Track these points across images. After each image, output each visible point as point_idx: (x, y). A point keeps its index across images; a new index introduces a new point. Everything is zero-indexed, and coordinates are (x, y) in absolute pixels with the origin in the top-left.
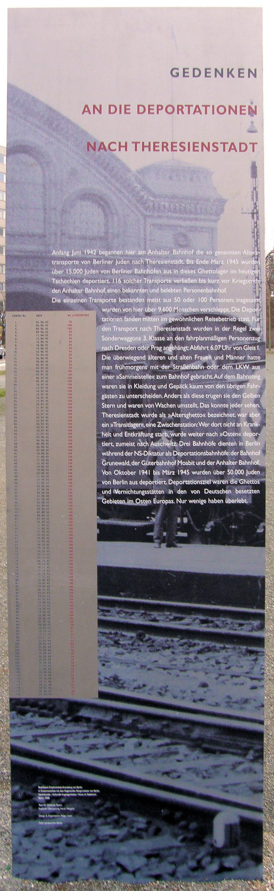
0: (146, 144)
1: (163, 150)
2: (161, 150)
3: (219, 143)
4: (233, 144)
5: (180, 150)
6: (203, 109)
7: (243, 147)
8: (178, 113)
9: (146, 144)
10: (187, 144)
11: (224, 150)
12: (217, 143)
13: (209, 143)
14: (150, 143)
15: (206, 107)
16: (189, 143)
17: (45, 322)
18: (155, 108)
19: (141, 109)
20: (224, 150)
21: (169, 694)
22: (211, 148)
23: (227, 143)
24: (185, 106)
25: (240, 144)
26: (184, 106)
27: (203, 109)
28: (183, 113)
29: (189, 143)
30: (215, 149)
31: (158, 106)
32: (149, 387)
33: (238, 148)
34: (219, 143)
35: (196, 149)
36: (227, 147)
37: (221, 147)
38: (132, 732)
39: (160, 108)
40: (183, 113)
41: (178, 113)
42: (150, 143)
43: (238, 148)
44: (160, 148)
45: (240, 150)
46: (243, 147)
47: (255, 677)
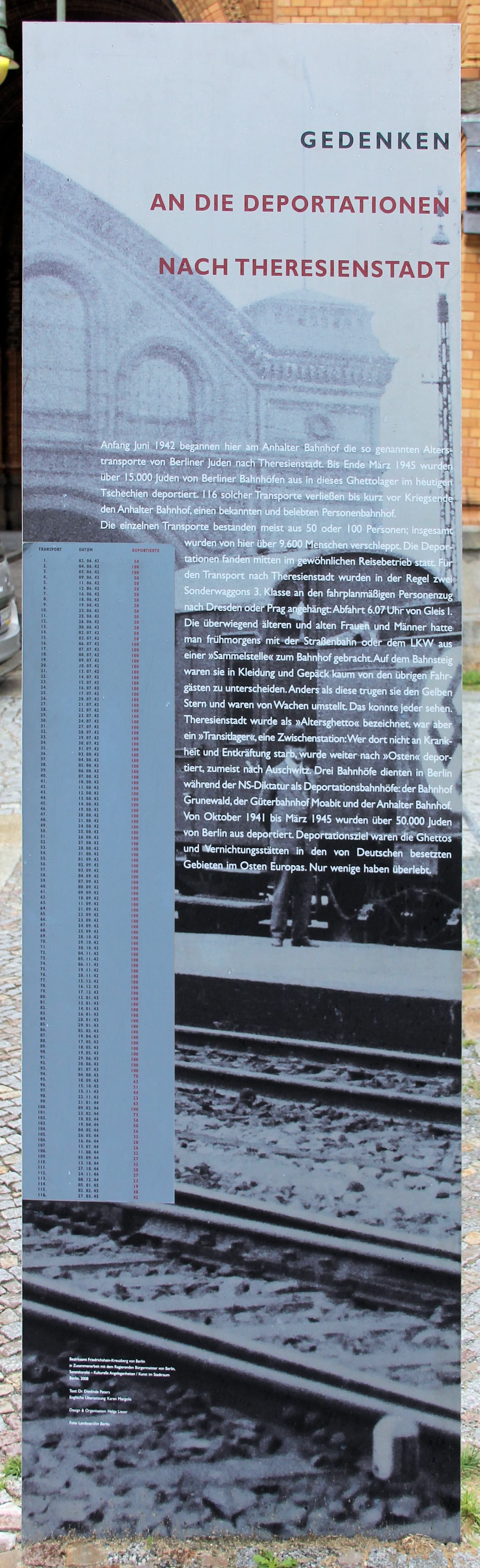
1: (288, 274)
2: (211, 271)
3: (384, 263)
6: (356, 204)
7: (425, 270)
8: (314, 210)
9: (260, 263)
11: (392, 275)
13: (366, 263)
14: (265, 261)
15: (362, 199)
16: (332, 262)
17: (93, 560)
18: (275, 200)
20: (392, 275)
22: (371, 270)
24: (327, 197)
25: (420, 264)
26: (324, 198)
27: (356, 204)
28: (322, 210)
29: (332, 262)
31: (280, 197)
33: (415, 272)
34: (384, 263)
36: (398, 268)
37: (386, 269)
41: (314, 210)
42: (265, 261)
43: (415, 272)
44: (350, 271)
45: (420, 276)
46: (425, 270)
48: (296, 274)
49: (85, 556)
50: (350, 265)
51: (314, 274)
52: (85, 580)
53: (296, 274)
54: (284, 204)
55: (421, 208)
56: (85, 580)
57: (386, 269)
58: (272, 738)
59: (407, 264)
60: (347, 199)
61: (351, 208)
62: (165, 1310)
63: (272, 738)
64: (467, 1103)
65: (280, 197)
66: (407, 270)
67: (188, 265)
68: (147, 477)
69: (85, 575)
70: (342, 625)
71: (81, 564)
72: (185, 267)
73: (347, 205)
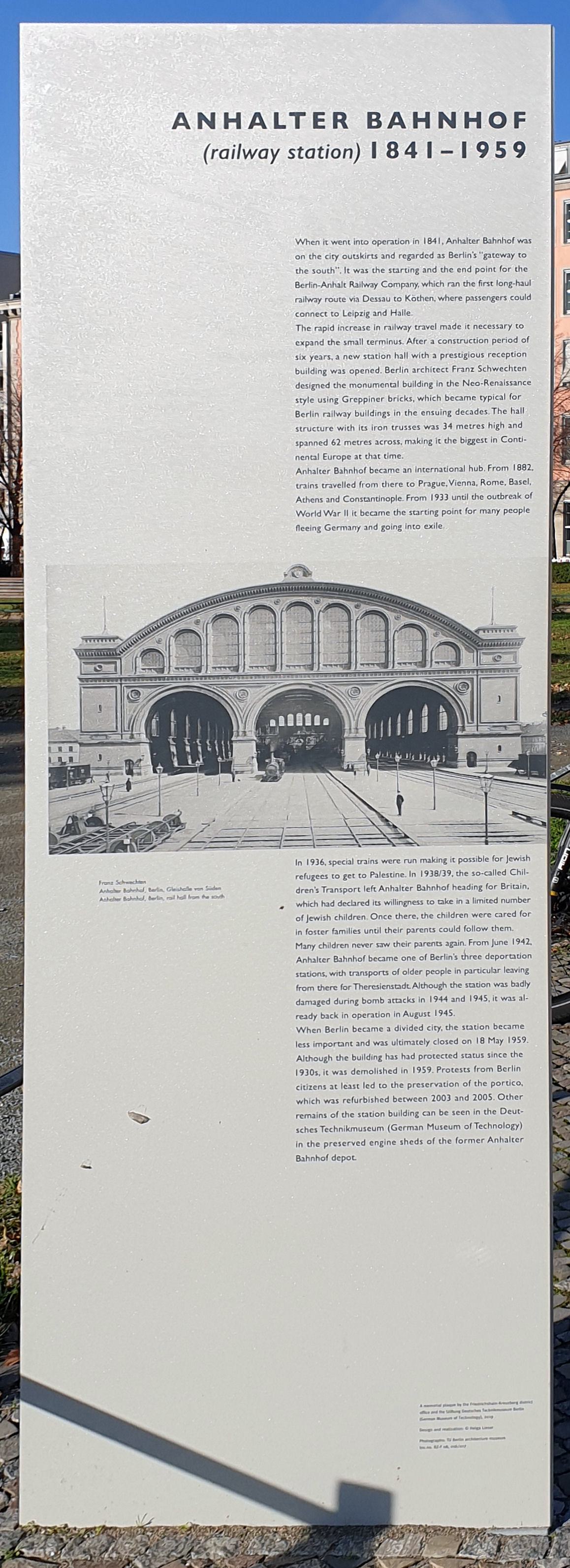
43: (270, 152)
45: (267, 150)
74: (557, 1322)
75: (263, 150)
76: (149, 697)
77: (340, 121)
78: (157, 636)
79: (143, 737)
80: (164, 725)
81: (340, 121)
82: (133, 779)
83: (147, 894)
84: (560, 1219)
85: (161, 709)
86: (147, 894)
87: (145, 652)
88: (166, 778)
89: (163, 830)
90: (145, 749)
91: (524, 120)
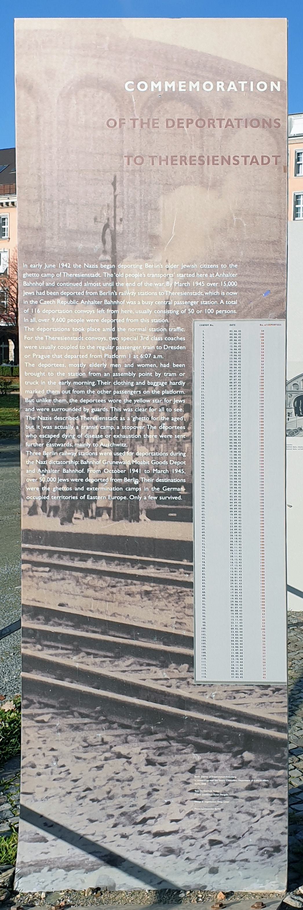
0: (164, 157)
1: (181, 164)
2: (179, 163)
3: (240, 157)
4: (254, 157)
5: (199, 164)
6: (235, 123)
7: (266, 161)
8: (209, 127)
9: (164, 157)
10: (206, 157)
11: (245, 164)
12: (238, 157)
13: (229, 157)
14: (167, 157)
15: (239, 120)
16: (208, 157)
17: (238, 331)
18: (185, 122)
19: (170, 123)
20: (245, 164)
21: (99, 663)
22: (232, 161)
23: (249, 156)
24: (217, 119)
25: (262, 157)
26: (215, 120)
27: (235, 123)
28: (214, 127)
29: (208, 157)
30: (236, 162)
31: (188, 120)
32: (127, 383)
33: (260, 161)
34: (240, 157)
35: (174, 162)
36: (249, 160)
37: (241, 160)
38: (224, 744)
39: (190, 121)
40: (214, 127)
41: (209, 127)
42: (167, 157)
43: (260, 161)
44: (220, 162)
45: (263, 164)
46: (266, 161)
47: (159, 678)
48: (186, 164)
49: (231, 328)
50: (220, 158)
51: (197, 164)
52: (233, 342)
53: (186, 164)
54: (190, 123)
55: (153, 125)
56: (233, 342)
57: (241, 160)
58: (76, 401)
59: (254, 157)
60: (229, 120)
61: (232, 125)
62: (141, 678)
63: (76, 401)
64: (197, 578)
65: (188, 120)
66: (254, 160)
67: (256, 159)
68: (231, 284)
69: (233, 339)
70: (25, 338)
71: (231, 333)
72: (254, 160)
73: (229, 123)
74: (285, 903)
75: (265, 164)
76: (295, 396)
77: (183, 160)
78: (297, 380)
79: (293, 407)
80: (298, 404)
81: (183, 160)
82: (290, 418)
83: (293, 448)
84: (284, 713)
85: (298, 399)
86: (293, 448)
87: (294, 384)
88: (299, 418)
89: (297, 431)
90: (293, 410)
91: (125, 123)
